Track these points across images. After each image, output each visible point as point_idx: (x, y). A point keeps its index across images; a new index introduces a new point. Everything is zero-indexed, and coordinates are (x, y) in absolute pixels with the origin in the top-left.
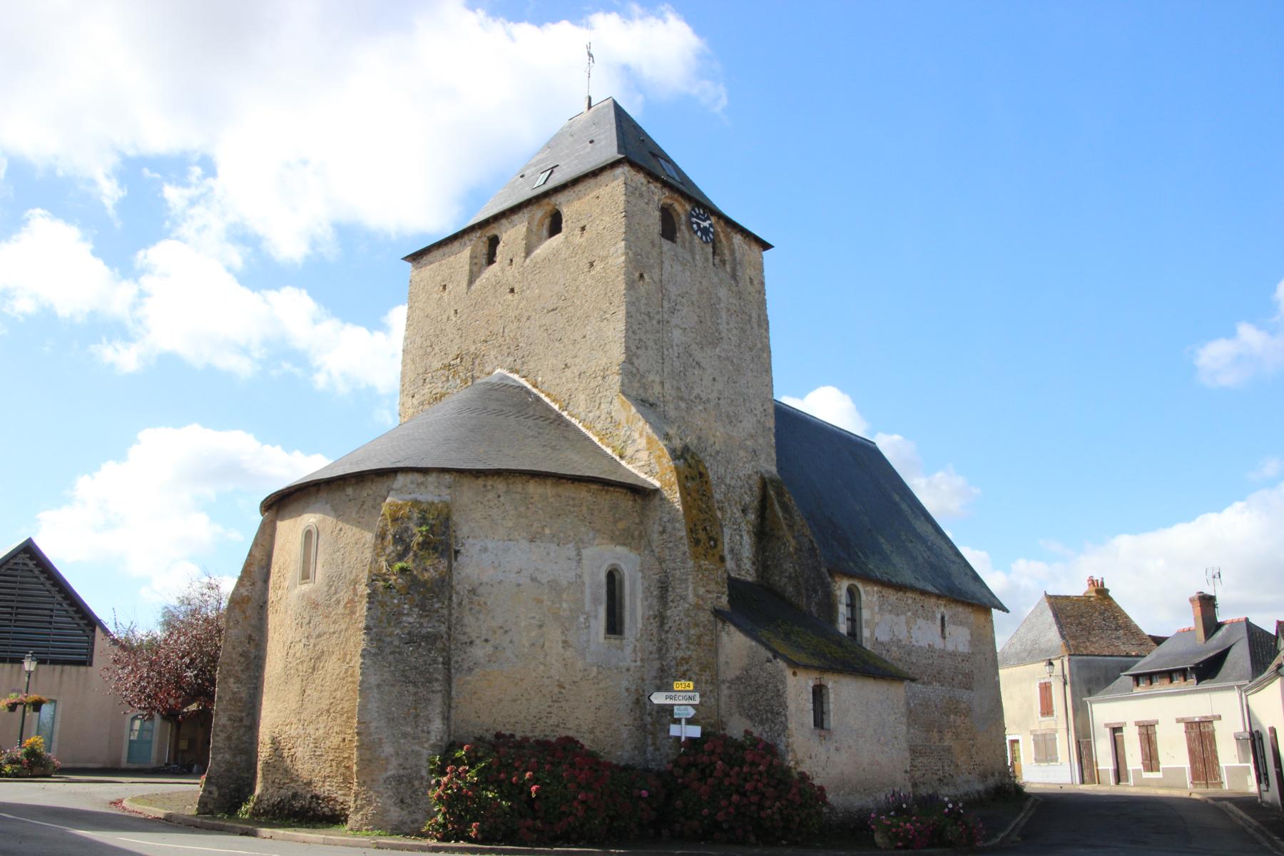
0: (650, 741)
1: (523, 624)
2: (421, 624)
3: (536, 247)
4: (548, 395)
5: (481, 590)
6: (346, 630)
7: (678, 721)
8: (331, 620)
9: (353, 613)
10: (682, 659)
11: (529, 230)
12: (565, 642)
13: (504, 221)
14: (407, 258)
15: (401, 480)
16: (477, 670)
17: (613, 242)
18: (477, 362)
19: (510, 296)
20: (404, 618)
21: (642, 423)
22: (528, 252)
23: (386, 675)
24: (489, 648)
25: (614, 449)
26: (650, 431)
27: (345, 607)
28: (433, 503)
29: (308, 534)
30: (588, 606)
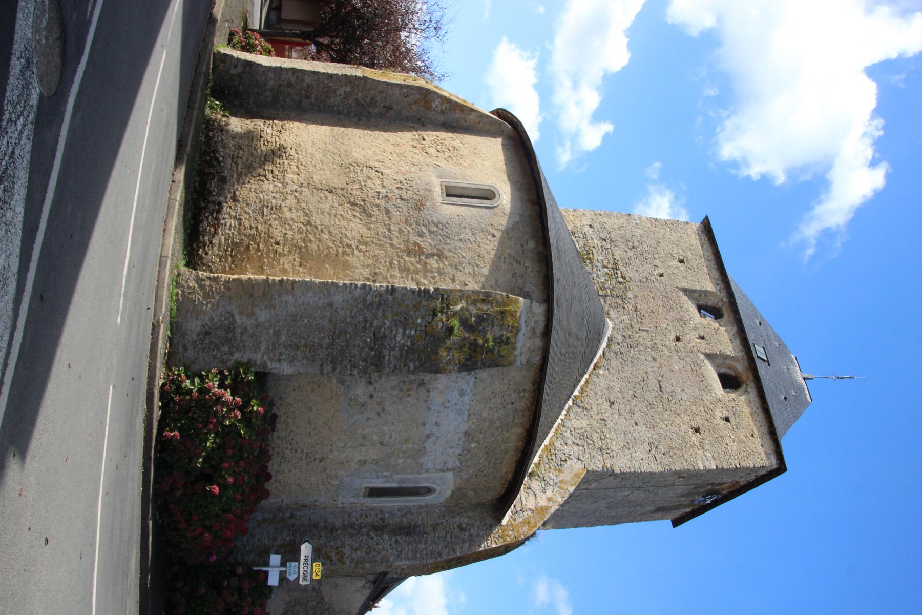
0: (266, 515)
1: (385, 428)
2: (393, 349)
4: (587, 382)
5: (422, 391)
6: (392, 245)
7: (283, 564)
8: (402, 226)
9: (409, 253)
11: (727, 357)
12: (365, 462)
13: (735, 329)
14: (707, 218)
15: (539, 309)
16: (342, 388)
17: (716, 455)
18: (619, 301)
19: (673, 337)
20: (400, 330)
21: (560, 500)
22: (709, 356)
23: (342, 313)
24: (363, 399)
25: (538, 465)
26: (552, 511)
27: (416, 244)
28: (515, 348)
29: (488, 195)
30: (396, 477)
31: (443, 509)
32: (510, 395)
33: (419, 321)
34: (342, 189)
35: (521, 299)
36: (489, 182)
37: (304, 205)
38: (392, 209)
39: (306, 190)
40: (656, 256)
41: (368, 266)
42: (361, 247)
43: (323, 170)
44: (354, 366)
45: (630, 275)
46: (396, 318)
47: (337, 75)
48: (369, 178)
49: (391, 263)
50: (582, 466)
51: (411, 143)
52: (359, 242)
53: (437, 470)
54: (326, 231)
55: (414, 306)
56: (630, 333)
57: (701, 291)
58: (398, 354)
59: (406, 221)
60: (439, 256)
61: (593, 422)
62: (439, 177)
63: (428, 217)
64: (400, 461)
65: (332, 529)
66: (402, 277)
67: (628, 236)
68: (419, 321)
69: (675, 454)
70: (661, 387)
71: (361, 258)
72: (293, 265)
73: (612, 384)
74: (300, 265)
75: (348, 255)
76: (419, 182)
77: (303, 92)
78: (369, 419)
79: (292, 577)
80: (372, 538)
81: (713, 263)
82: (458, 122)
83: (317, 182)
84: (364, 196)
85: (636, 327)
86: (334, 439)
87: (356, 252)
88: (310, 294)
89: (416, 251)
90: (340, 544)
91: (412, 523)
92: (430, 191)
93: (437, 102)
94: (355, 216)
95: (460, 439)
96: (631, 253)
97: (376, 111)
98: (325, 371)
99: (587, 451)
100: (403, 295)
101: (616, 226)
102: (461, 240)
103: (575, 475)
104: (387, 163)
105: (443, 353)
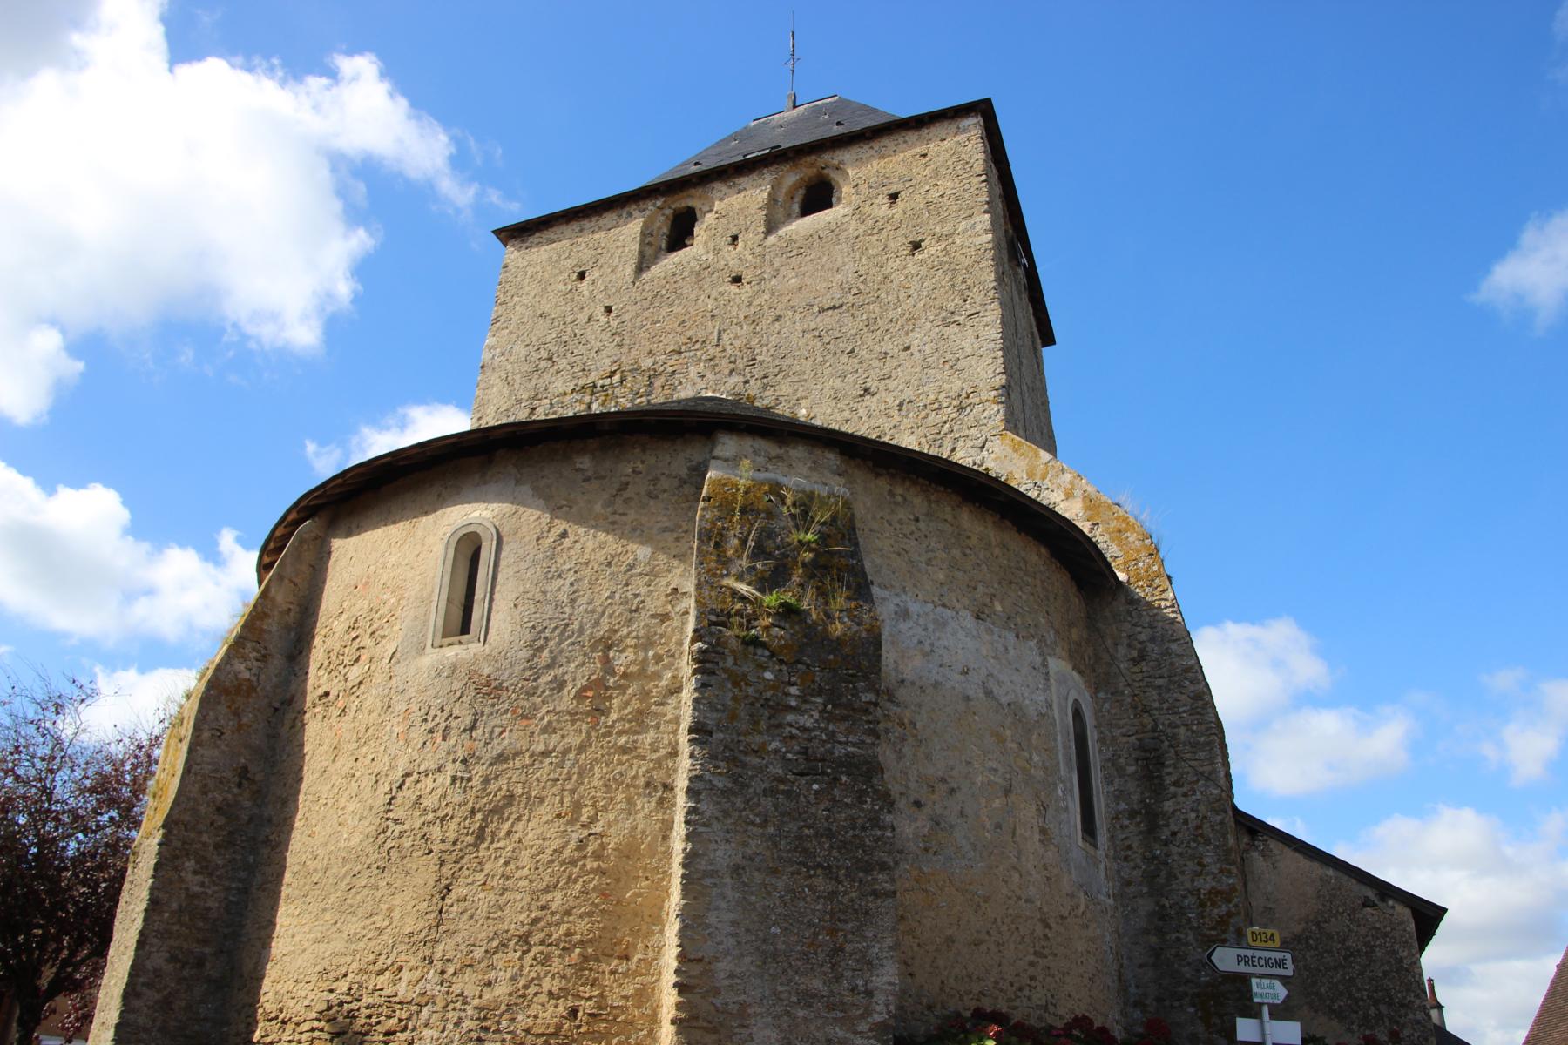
2: (832, 735)
3: (784, 223)
6: (581, 749)
7: (1253, 1012)
8: (535, 725)
9: (599, 711)
10: (1214, 892)
11: (772, 199)
12: (1043, 831)
13: (717, 185)
14: (497, 232)
15: (728, 445)
19: (733, 287)
20: (790, 718)
22: (771, 228)
23: (754, 845)
27: (580, 696)
29: (469, 551)
31: (1101, 695)
32: (900, 522)
33: (768, 675)
34: (442, 863)
35: (711, 474)
36: (439, 549)
37: (479, 953)
38: (496, 748)
39: (440, 948)
40: (569, 319)
41: (630, 801)
42: (584, 819)
43: (391, 909)
44: (875, 822)
45: (606, 364)
46: (763, 726)
47: (152, 889)
48: (417, 802)
49: (624, 750)
50: (997, 441)
51: (333, 720)
52: (572, 822)
53: (1047, 688)
54: (545, 898)
55: (736, 684)
56: (725, 362)
57: (642, 243)
58: (843, 727)
59: (524, 717)
60: (609, 648)
61: (906, 423)
62: (421, 651)
63: (517, 669)
64: (1036, 758)
65: (1162, 918)
66: (657, 727)
67: (526, 367)
68: (768, 675)
69: (964, 282)
70: (834, 308)
71: (611, 817)
72: (626, 974)
73: (828, 392)
74: (627, 958)
75: (603, 847)
76: (432, 692)
77: (185, 973)
78: (962, 814)
79: (1281, 992)
80: (1174, 834)
81: (586, 224)
82: (288, 628)
83: (421, 924)
84: (463, 812)
85: (712, 351)
86: (1005, 891)
87: (597, 828)
88: (712, 918)
89: (596, 697)
90: (1190, 901)
91: (1135, 754)
92: (454, 668)
93: (240, 666)
94: (509, 833)
95: (990, 631)
96: (562, 363)
97: (247, 804)
98: (888, 886)
99: (967, 432)
100: (713, 708)
101: (506, 390)
102: (573, 601)
103: (1016, 451)
104: (382, 765)
105: (837, 629)
